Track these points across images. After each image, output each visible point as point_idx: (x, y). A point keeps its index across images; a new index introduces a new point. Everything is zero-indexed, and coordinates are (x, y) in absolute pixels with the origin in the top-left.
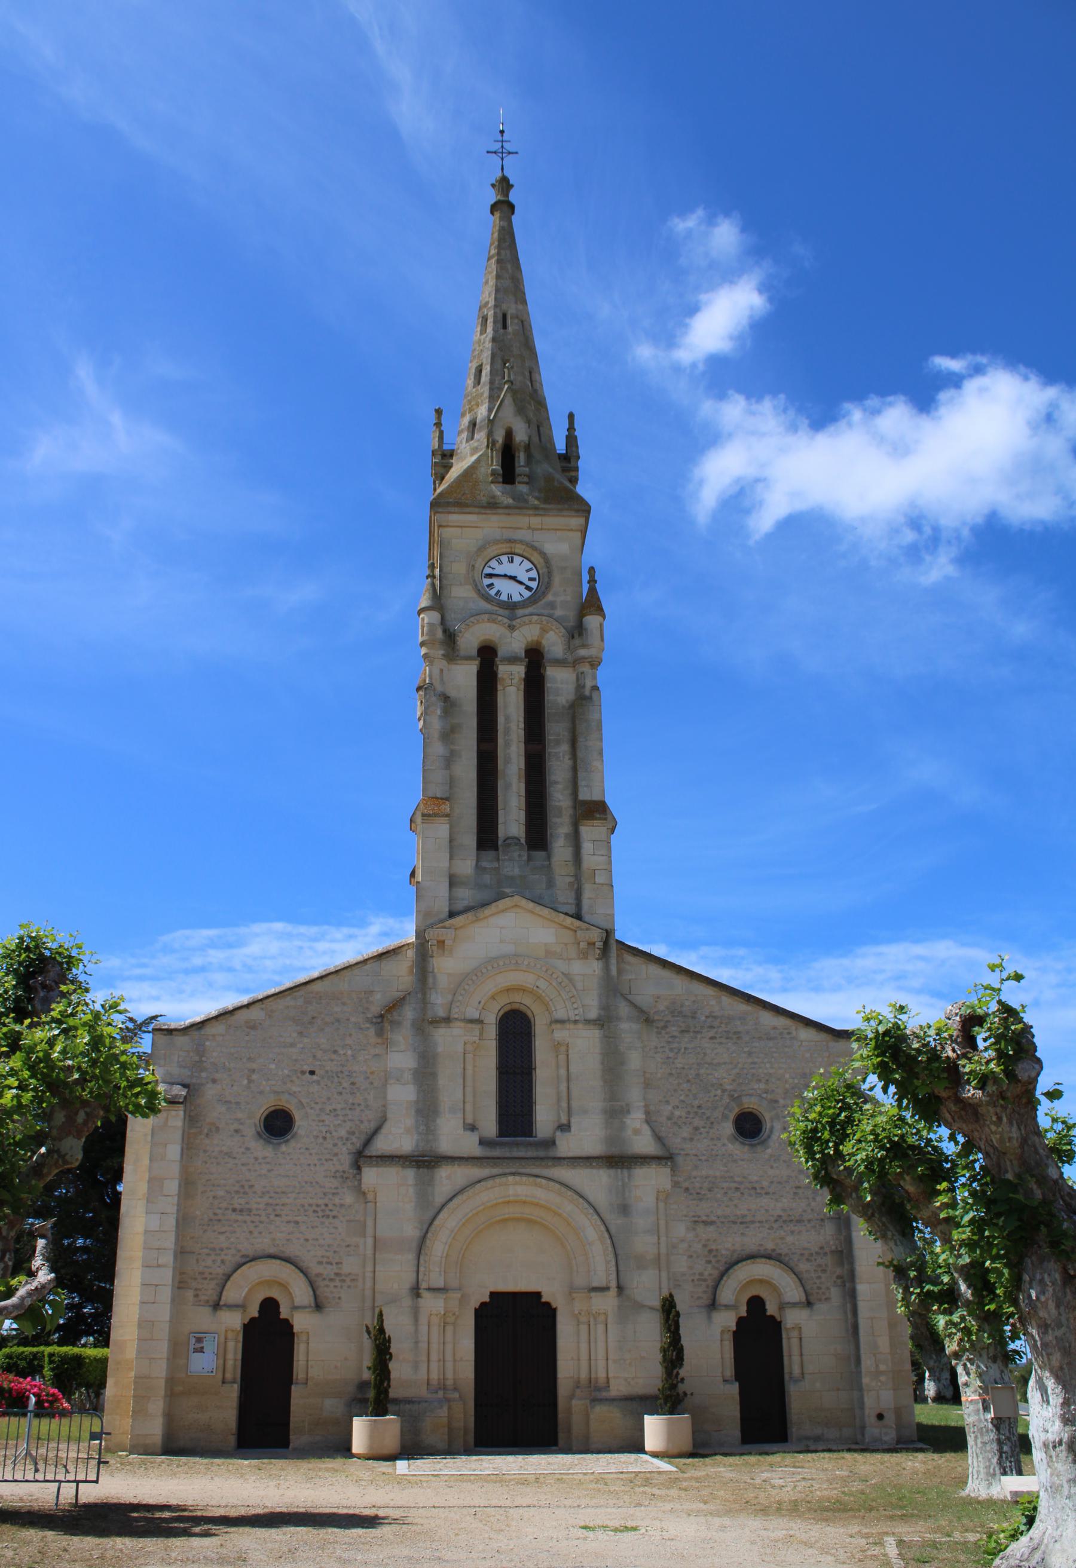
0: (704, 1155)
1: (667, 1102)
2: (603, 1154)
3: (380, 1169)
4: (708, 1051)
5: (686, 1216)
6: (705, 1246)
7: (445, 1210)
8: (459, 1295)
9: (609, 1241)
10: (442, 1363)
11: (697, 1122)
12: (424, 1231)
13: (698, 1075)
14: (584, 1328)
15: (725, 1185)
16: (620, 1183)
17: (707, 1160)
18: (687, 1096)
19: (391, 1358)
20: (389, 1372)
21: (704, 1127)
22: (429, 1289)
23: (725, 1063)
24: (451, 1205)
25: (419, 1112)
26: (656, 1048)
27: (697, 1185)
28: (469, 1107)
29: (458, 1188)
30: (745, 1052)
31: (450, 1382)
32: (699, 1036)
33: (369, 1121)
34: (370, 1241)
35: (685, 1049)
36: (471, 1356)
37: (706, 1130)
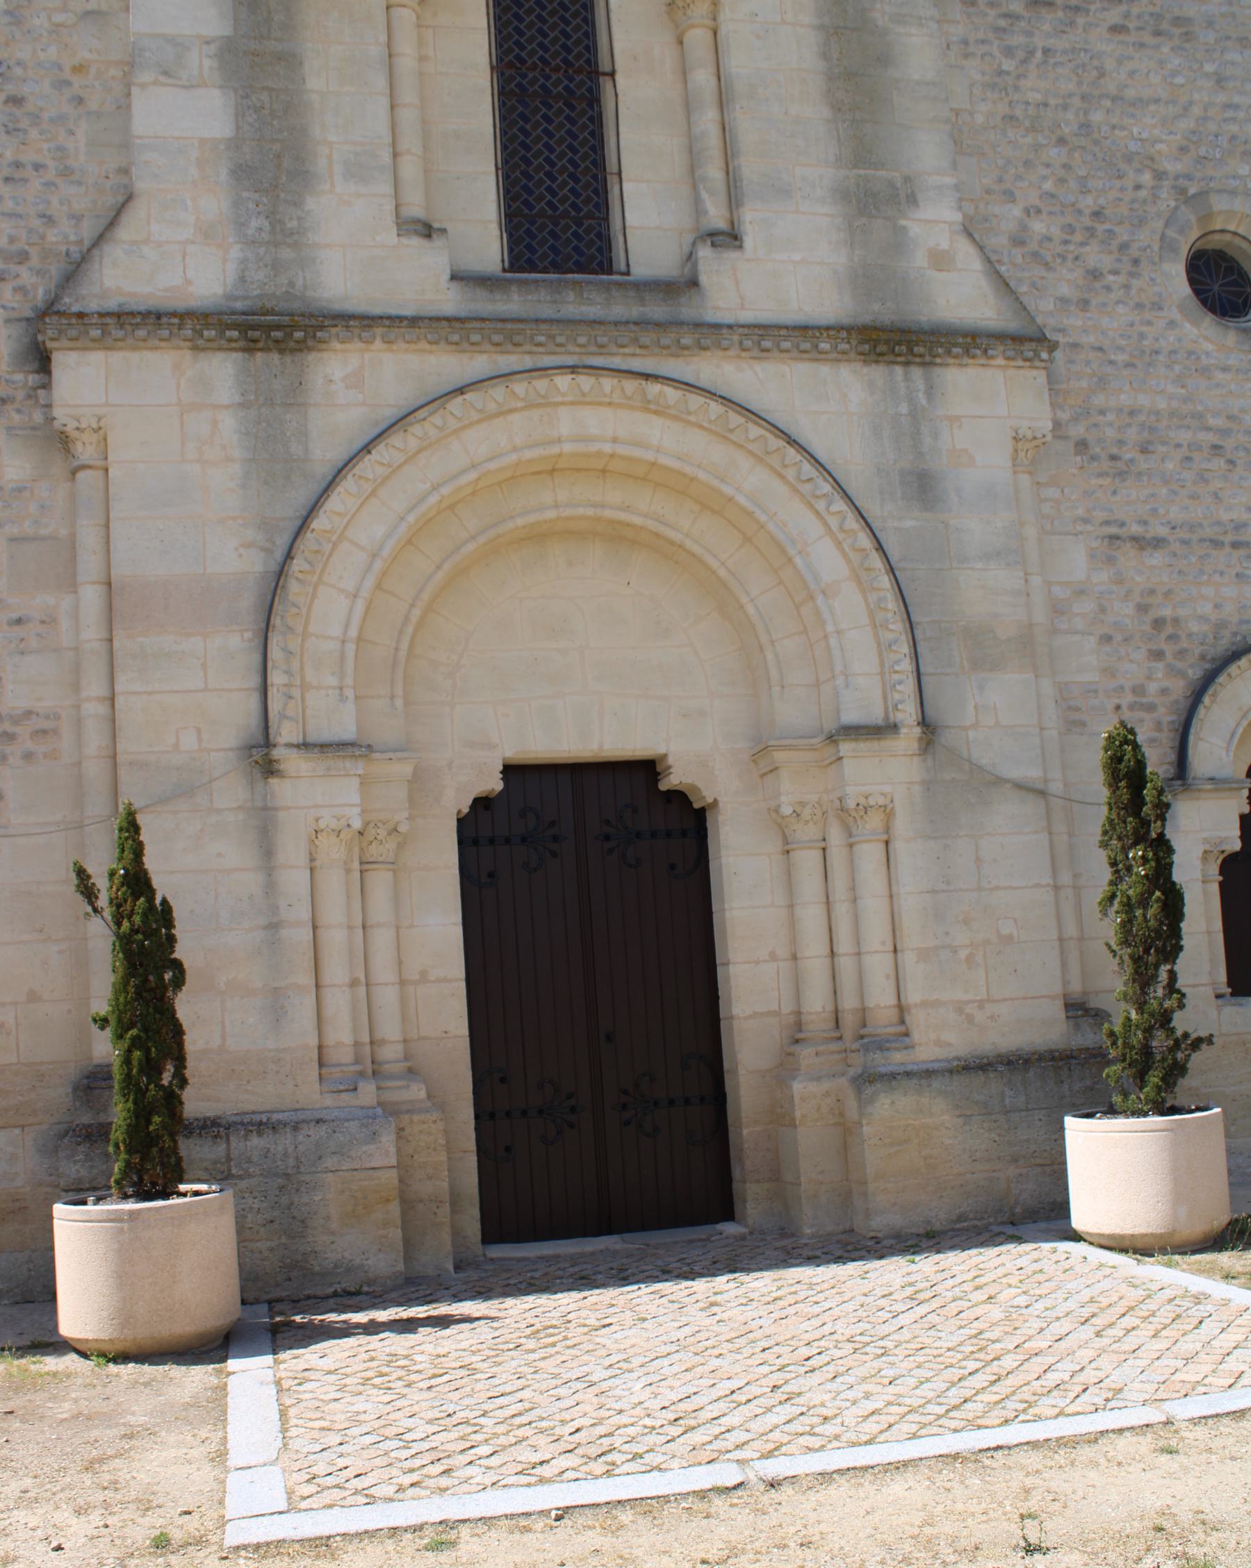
0: (1120, 349)
1: (1010, 196)
2: (846, 321)
3: (117, 357)
4: (1109, 64)
5: (1086, 521)
6: (1143, 608)
7: (348, 484)
8: (407, 769)
9: (885, 581)
10: (362, 990)
11: (1095, 256)
12: (279, 554)
13: (1086, 127)
14: (808, 860)
15: (1185, 436)
16: (904, 409)
17: (1128, 365)
18: (1062, 181)
19: (179, 981)
20: (178, 1031)
21: (1115, 272)
22: (305, 746)
23: (1157, 101)
24: (367, 466)
25: (243, 173)
26: (965, 42)
27: (1110, 433)
28: (410, 168)
29: (389, 414)
30: (1207, 75)
31: (391, 1052)
32: (1081, 21)
33: (77, 218)
34: (91, 596)
35: (1046, 51)
36: (456, 967)
37: (1121, 279)
